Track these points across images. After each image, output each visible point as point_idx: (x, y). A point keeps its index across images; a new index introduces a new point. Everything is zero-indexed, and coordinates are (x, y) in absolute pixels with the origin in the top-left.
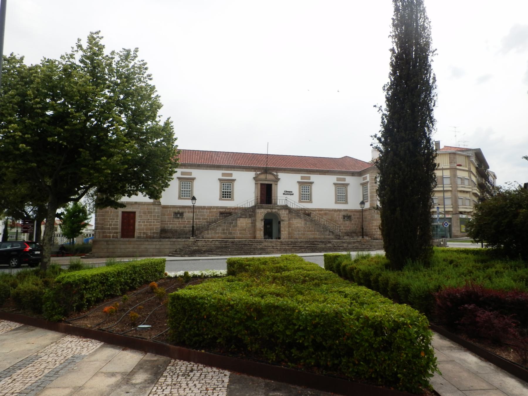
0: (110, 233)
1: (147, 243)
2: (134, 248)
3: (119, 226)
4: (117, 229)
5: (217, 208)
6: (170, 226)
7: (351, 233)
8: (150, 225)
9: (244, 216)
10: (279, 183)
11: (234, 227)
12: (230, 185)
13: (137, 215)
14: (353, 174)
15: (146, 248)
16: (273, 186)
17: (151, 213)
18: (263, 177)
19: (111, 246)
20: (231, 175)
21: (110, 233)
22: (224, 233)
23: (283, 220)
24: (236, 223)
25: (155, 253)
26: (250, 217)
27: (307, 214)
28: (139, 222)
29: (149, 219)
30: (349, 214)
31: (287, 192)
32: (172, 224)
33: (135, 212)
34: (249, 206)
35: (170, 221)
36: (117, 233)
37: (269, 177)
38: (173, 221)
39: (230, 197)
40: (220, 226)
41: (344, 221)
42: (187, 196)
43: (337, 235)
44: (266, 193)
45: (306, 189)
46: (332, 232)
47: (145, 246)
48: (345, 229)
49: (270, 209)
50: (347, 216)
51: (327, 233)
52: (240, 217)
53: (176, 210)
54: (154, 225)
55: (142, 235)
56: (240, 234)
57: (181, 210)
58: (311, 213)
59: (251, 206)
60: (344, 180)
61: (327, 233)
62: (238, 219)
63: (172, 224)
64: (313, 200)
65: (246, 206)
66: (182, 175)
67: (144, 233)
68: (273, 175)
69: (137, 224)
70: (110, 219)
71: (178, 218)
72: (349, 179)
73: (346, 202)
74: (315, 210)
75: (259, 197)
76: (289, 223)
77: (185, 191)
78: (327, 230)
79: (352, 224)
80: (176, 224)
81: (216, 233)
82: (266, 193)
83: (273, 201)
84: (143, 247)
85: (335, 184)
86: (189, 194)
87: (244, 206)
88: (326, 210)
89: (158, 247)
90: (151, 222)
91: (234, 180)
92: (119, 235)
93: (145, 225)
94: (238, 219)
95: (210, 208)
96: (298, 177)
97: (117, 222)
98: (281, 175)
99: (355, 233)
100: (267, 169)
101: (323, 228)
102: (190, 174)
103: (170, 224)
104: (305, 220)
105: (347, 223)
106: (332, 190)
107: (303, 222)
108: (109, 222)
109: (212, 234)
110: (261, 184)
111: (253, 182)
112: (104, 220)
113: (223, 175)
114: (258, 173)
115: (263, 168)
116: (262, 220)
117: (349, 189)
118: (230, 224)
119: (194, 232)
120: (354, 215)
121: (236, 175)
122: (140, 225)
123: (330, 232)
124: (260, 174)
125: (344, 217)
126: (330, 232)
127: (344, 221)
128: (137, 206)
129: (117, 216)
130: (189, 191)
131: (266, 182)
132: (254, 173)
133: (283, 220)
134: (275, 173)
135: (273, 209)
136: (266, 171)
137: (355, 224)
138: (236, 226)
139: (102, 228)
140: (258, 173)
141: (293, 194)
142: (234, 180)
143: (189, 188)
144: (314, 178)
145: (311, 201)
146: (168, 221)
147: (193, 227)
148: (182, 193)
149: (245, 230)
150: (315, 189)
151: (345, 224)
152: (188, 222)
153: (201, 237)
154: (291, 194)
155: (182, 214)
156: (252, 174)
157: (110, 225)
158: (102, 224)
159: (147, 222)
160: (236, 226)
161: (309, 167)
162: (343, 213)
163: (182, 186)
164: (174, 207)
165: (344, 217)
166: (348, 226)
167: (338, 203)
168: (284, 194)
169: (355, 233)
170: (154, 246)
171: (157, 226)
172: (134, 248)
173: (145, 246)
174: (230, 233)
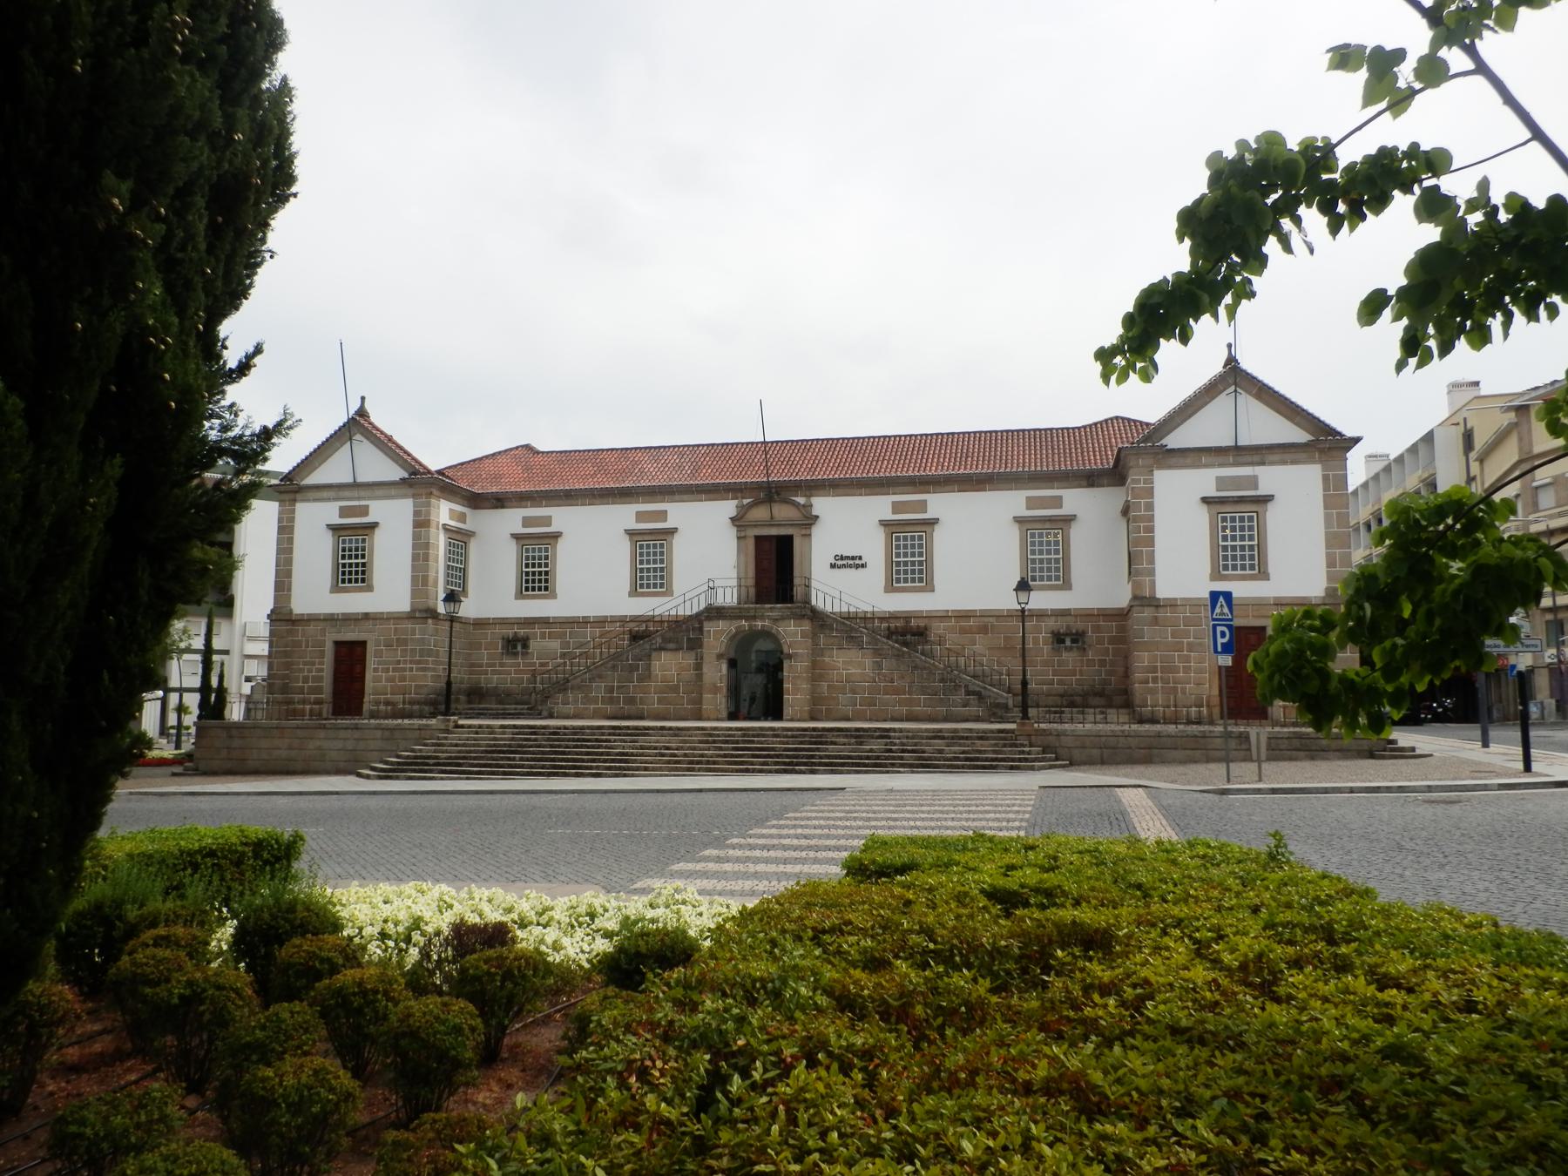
0: (304, 702)
1: (322, 734)
2: (290, 748)
3: (327, 684)
4: (318, 690)
5: (623, 620)
6: (492, 680)
7: (1085, 695)
8: (403, 679)
9: (671, 646)
10: (817, 532)
11: (640, 679)
12: (662, 546)
13: (370, 649)
14: (1091, 479)
15: (319, 748)
16: (797, 542)
17: (404, 642)
18: (760, 513)
19: (236, 743)
20: (662, 516)
21: (304, 702)
22: (611, 701)
23: (790, 657)
24: (648, 668)
25: (342, 765)
26: (690, 648)
27: (906, 635)
28: (376, 670)
29: (398, 662)
30: (1079, 625)
31: (842, 558)
32: (499, 673)
33: (363, 644)
34: (688, 613)
35: (494, 665)
36: (319, 702)
37: (782, 512)
38: (502, 665)
39: (546, 589)
40: (600, 677)
41: (1056, 651)
42: (913, 580)
43: (998, 705)
44: (775, 567)
45: (651, 556)
46: (978, 694)
47: (318, 743)
48: (1060, 682)
49: (747, 618)
50: (1070, 634)
51: (960, 696)
52: (661, 649)
53: (510, 633)
54: (413, 679)
55: (382, 707)
56: (660, 701)
57: (522, 632)
58: (926, 628)
59: (695, 611)
60: (1057, 502)
61: (960, 696)
62: (654, 654)
63: (499, 673)
64: (1271, 570)
65: (681, 613)
66: (524, 526)
67: (387, 703)
68: (796, 505)
69: (369, 675)
70: (305, 664)
71: (515, 654)
72: (1074, 500)
73: (1067, 585)
74: (944, 616)
75: (751, 582)
76: (814, 665)
77: (906, 564)
78: (957, 687)
79: (1090, 663)
80: (507, 674)
81: (587, 700)
82: (775, 567)
83: (798, 591)
84: (312, 745)
85: (1019, 520)
86: (921, 571)
87: (673, 613)
88: (985, 614)
89: (350, 745)
90: (404, 670)
91: (672, 532)
92: (326, 709)
93: (388, 680)
94: (654, 654)
95: (602, 621)
96: (881, 506)
97: (321, 670)
98: (822, 505)
99: (1100, 694)
100: (774, 493)
101: (942, 680)
102: (547, 521)
103: (494, 673)
104: (877, 653)
105: (1070, 658)
106: (620, 555)
107: (868, 662)
108: (301, 670)
109: (576, 702)
110: (758, 538)
111: (730, 534)
112: (288, 666)
113: (640, 516)
114: (746, 501)
115: (758, 487)
116: (720, 657)
117: (1077, 533)
118: (631, 671)
119: (533, 700)
120: (1097, 629)
121: (678, 513)
122: (377, 679)
123: (968, 693)
124: (751, 506)
125: (1058, 638)
126: (968, 693)
127: (1056, 651)
128: (369, 625)
129: (322, 654)
130: (921, 563)
131: (774, 532)
132: (735, 502)
133: (790, 657)
134: (801, 500)
135: (754, 618)
136: (772, 493)
137: (1102, 663)
138: (647, 676)
139: (285, 689)
140: (746, 501)
141: (863, 566)
142: (672, 532)
143: (921, 554)
144: (938, 504)
145: (929, 587)
146: (489, 665)
147: (449, 683)
148: (642, 578)
149: (675, 689)
150: (942, 542)
151: (1060, 663)
152: (542, 665)
153: (545, 713)
154: (857, 566)
155: (525, 642)
156: (728, 507)
157: (306, 680)
158: (286, 677)
159: (394, 670)
160: (649, 676)
161: (916, 471)
162: (1051, 623)
163: (641, 554)
164: (504, 622)
165: (1058, 638)
166: (1075, 668)
167: (528, 597)
168: (833, 566)
169: (1100, 694)
170: (340, 744)
171: (429, 680)
172: (290, 748)
173: (318, 743)
174: (632, 701)
